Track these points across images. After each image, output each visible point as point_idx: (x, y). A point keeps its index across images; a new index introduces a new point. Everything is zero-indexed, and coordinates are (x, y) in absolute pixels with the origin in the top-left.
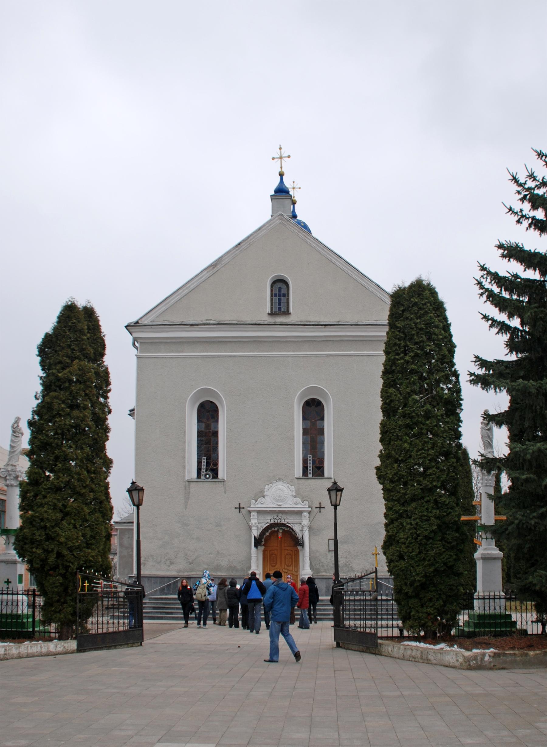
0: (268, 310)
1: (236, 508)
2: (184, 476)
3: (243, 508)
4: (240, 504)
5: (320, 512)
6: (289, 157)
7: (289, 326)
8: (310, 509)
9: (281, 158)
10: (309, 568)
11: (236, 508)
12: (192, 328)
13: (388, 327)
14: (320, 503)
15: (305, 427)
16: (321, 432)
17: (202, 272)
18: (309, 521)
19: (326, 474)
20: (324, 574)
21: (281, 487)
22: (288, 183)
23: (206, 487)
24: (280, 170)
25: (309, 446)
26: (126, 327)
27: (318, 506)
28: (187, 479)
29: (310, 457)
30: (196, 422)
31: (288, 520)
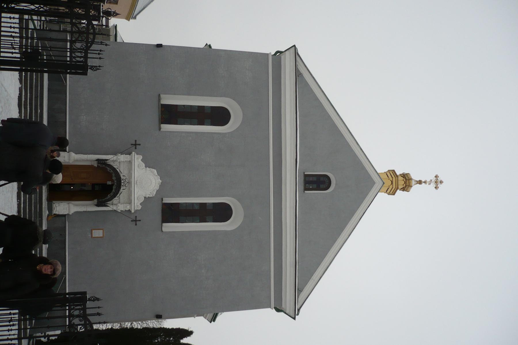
1: (136, 141)
8: (133, 211)
11: (136, 141)
23: (155, 115)
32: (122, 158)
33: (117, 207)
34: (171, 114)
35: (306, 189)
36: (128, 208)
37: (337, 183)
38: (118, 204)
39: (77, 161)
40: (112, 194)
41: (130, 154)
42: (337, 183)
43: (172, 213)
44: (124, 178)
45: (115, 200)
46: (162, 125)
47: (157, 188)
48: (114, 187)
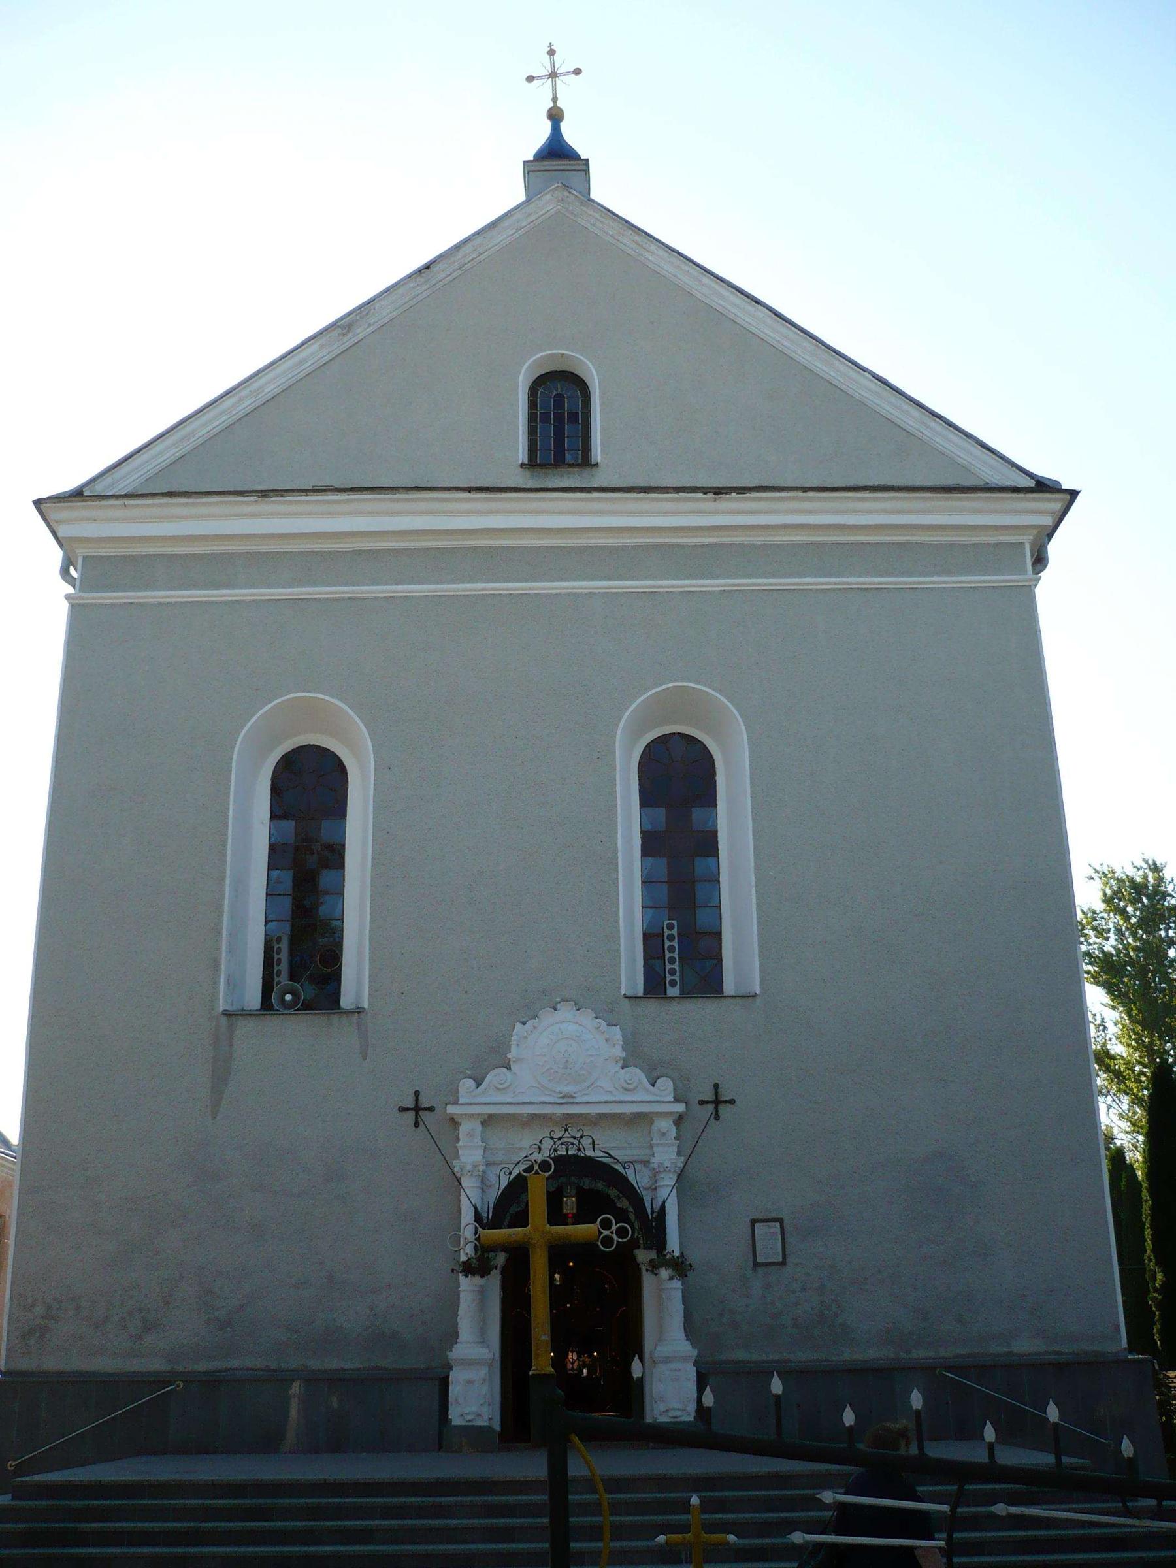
0: (522, 455)
1: (403, 1110)
2: (214, 999)
3: (431, 1109)
4: (417, 1094)
5: (717, 1117)
6: (577, 72)
7: (595, 495)
8: (680, 1108)
9: (554, 75)
10: (681, 1334)
11: (403, 1110)
12: (268, 505)
13: (665, 887)
14: (716, 1086)
15: (649, 827)
16: (708, 844)
17: (303, 344)
18: (679, 1153)
19: (729, 987)
20: (740, 1355)
21: (572, 1027)
22: (572, 135)
23: (296, 1032)
24: (551, 105)
25: (663, 893)
26: (38, 503)
27: (709, 1096)
28: (221, 1006)
29: (671, 927)
30: (267, 815)
31: (608, 1145)
32: (470, 1154)
33: (666, 1170)
34: (305, 963)
35: (586, 461)
36: (666, 1125)
37: (558, 358)
38: (654, 1165)
39: (482, 1332)
40: (613, 1193)
41: (454, 1122)
42: (558, 358)
43: (684, 952)
44: (547, 1144)
45: (638, 1178)
46: (346, 1001)
47: (587, 1018)
48: (587, 1184)
